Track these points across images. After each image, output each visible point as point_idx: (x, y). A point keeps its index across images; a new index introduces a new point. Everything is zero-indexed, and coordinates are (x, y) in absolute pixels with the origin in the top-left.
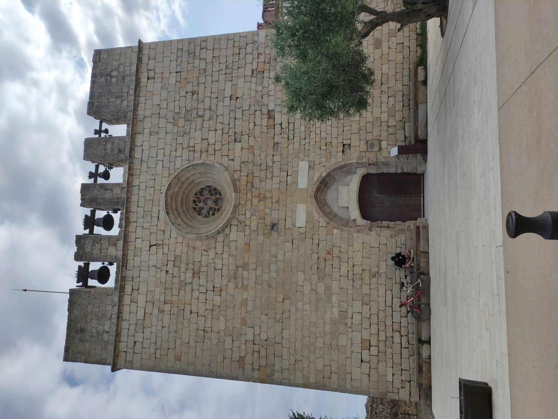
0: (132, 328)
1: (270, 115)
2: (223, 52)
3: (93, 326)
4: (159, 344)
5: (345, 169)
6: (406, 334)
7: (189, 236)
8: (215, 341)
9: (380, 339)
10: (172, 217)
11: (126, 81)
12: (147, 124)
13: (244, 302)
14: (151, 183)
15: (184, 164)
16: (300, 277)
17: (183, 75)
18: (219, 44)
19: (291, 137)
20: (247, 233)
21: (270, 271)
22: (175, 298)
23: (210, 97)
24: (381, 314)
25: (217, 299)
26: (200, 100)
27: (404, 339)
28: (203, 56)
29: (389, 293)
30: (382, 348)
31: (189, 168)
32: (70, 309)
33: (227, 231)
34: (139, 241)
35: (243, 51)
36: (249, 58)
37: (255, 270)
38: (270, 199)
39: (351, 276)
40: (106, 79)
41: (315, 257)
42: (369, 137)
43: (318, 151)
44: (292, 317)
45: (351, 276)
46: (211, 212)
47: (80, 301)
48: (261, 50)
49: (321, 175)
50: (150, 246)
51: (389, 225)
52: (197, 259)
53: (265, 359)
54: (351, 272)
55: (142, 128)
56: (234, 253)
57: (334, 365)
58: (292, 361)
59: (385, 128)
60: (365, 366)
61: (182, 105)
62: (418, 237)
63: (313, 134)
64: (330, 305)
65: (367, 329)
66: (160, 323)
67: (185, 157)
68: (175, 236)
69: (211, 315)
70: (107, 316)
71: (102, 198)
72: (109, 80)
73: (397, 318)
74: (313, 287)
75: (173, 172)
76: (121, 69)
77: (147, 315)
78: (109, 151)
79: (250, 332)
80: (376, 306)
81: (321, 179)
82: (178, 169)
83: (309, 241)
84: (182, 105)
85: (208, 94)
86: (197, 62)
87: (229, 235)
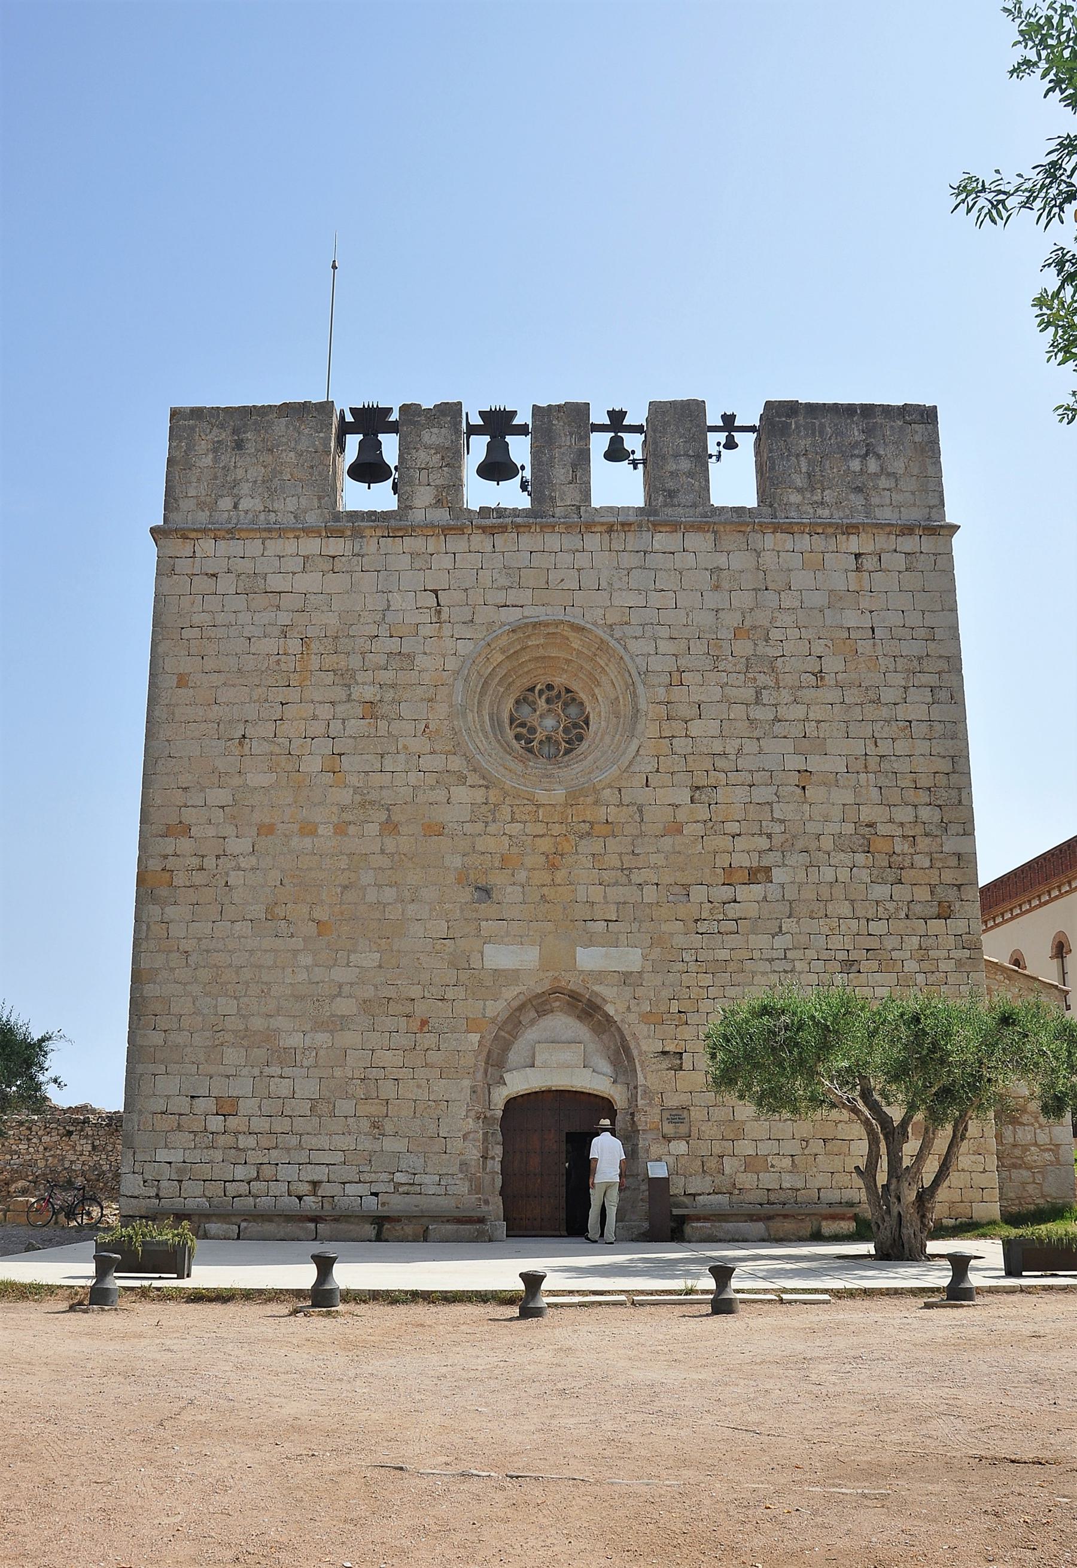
0: (246, 566)
1: (757, 875)
2: (923, 747)
3: (249, 469)
4: (211, 633)
5: (622, 1059)
6: (254, 1191)
7: (460, 685)
8: (221, 764)
9: (240, 1137)
10: (504, 641)
11: (852, 496)
12: (740, 560)
13: (308, 830)
14: (589, 581)
15: (638, 660)
16: (369, 959)
17: (865, 647)
18: (943, 736)
19: (703, 927)
20: (468, 828)
21: (380, 886)
22: (314, 662)
23: (807, 719)
24: (294, 1140)
25: (313, 765)
26: (799, 693)
27: (243, 1188)
28: (914, 695)
29: (339, 1157)
30: (222, 1140)
31: (627, 675)
32: (288, 410)
33: (473, 779)
34: (447, 562)
35: (923, 797)
36: (904, 814)
37: (382, 852)
38: (549, 881)
39: (374, 1073)
40: (857, 443)
41: (415, 992)
42: (696, 1114)
43: (666, 993)
44: (279, 941)
45: (374, 1073)
46: (524, 731)
47: (306, 431)
48: (923, 843)
49: (606, 1002)
50: (435, 592)
51: (493, 1158)
52: (405, 710)
53: (188, 884)
54: (381, 1074)
55: (730, 548)
56: (421, 798)
57: (179, 1038)
58: (185, 945)
59: (717, 1150)
60: (184, 1104)
61: (789, 647)
62: (459, 1221)
63: (707, 980)
64: (307, 1027)
65: (260, 1107)
66: (258, 632)
67: (655, 664)
68: (461, 651)
69: (278, 752)
70: (273, 501)
71: (552, 458)
72: (856, 452)
73: (286, 1173)
74: (346, 989)
75: (618, 634)
76: (883, 482)
77: (274, 599)
78: (671, 466)
79: (243, 845)
80: (310, 1130)
81: (598, 1001)
82: (625, 648)
83: (451, 976)
84: (789, 647)
85: (816, 713)
86: (898, 680)
87: (464, 784)
